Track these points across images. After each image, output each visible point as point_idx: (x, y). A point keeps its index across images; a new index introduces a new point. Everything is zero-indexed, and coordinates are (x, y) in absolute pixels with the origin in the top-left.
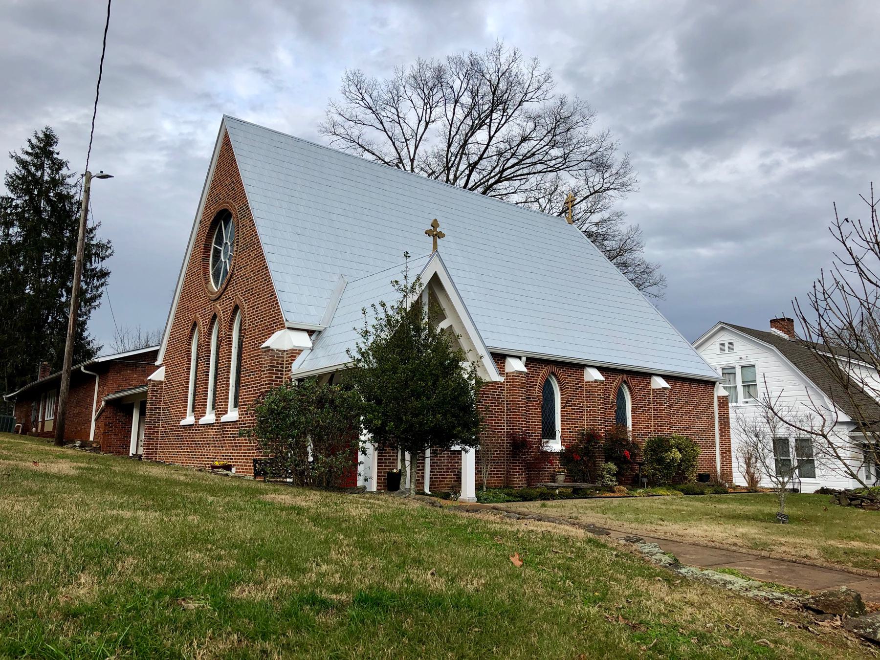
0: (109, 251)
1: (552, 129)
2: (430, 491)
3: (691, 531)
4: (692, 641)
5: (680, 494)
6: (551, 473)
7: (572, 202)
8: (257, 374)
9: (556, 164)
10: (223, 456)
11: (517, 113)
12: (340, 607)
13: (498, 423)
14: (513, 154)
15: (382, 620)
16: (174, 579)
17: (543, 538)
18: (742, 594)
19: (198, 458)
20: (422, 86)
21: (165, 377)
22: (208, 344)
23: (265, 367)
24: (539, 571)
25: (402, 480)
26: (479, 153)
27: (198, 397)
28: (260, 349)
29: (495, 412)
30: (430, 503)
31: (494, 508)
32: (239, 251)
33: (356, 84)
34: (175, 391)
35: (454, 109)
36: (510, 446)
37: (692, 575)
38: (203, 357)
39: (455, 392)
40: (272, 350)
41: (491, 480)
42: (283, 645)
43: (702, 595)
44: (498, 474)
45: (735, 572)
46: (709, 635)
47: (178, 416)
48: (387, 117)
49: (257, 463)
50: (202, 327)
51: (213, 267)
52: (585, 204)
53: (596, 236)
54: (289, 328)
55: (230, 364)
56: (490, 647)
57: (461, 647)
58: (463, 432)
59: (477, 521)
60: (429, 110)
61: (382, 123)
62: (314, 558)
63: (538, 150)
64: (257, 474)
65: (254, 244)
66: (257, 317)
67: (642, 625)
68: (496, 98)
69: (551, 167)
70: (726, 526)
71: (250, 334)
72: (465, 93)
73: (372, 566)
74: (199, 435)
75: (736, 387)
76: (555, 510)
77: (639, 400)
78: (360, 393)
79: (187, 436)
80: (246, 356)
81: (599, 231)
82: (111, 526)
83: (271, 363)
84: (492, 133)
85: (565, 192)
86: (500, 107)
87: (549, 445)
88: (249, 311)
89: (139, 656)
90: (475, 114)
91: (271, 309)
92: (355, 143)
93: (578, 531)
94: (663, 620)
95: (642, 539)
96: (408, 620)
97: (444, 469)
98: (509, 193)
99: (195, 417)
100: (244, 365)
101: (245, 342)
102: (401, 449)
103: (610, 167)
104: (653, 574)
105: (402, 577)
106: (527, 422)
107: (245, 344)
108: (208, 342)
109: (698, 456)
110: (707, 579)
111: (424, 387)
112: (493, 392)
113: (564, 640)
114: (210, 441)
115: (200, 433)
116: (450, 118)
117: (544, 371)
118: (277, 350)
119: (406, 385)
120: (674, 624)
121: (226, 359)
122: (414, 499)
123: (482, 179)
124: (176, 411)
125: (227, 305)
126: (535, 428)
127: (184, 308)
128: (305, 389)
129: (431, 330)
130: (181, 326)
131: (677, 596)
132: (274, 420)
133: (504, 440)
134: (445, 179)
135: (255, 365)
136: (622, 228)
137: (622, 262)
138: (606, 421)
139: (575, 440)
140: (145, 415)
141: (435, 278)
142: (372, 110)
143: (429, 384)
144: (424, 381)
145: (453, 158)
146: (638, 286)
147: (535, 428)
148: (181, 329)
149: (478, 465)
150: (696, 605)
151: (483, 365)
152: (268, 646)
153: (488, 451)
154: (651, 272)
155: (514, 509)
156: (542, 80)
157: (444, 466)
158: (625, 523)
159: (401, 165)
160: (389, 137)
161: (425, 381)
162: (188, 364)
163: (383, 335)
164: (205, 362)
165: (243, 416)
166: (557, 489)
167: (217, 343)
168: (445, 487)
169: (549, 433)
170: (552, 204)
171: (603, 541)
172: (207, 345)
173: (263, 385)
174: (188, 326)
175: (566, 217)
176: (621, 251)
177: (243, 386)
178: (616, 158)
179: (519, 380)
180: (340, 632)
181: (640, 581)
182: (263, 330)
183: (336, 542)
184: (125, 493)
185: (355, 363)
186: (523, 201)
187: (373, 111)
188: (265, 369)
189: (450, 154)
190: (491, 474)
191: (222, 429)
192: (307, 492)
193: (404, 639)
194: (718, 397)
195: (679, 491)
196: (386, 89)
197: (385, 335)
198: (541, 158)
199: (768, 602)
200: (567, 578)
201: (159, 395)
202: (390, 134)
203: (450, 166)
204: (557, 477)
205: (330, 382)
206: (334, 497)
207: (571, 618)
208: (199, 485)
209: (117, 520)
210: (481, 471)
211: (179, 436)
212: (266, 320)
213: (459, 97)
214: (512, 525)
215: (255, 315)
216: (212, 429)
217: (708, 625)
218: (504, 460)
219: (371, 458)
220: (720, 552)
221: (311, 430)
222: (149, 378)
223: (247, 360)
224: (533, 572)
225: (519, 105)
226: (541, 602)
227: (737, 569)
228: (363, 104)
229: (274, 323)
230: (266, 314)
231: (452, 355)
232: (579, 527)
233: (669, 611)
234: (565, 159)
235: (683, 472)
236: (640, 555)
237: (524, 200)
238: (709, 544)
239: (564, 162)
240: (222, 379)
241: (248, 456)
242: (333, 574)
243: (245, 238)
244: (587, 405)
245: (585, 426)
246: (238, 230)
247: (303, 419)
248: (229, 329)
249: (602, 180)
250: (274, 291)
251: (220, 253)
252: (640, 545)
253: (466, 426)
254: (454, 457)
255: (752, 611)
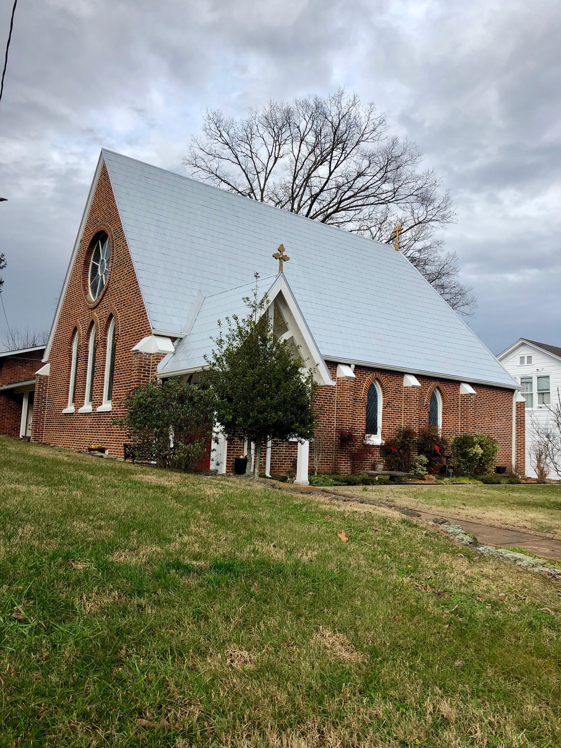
0: (3, 263)
1: (384, 166)
2: (270, 475)
3: (488, 515)
4: (487, 607)
5: (480, 483)
6: (372, 463)
7: (399, 231)
8: (127, 373)
9: (386, 198)
10: (98, 440)
11: (354, 151)
12: (200, 571)
13: (329, 420)
14: (350, 188)
15: (234, 583)
16: (65, 544)
17: (365, 518)
18: (529, 569)
19: (77, 441)
20: (272, 125)
21: (50, 372)
22: (87, 346)
23: (134, 367)
24: (362, 545)
25: (248, 466)
26: (320, 186)
27: (78, 390)
28: (130, 352)
29: (327, 410)
30: (271, 485)
31: (324, 491)
32: (113, 267)
33: (216, 122)
34: (59, 385)
35: (300, 147)
36: (338, 439)
37: (488, 553)
38: (82, 357)
39: (294, 394)
40: (141, 353)
41: (322, 467)
42: (155, 601)
43: (496, 569)
44: (327, 462)
45: (524, 550)
46: (500, 602)
47: (61, 405)
48: (242, 152)
49: (127, 447)
50: (81, 331)
51: (91, 281)
52: (410, 233)
53: (419, 261)
54: (155, 335)
55: (105, 363)
56: (322, 608)
57: (298, 607)
58: (300, 427)
59: (312, 501)
60: (278, 147)
61: (237, 157)
62: (177, 530)
63: (372, 184)
64: (126, 456)
65: (127, 262)
66: (128, 324)
67: (446, 593)
68: (336, 138)
69: (382, 200)
70: (518, 511)
71: (122, 339)
72: (310, 133)
73: (225, 538)
74: (78, 422)
75: (532, 394)
76: (374, 493)
77: (449, 403)
78: (215, 392)
79: (68, 422)
80: (119, 357)
81: (421, 257)
82: (11, 498)
83: (140, 364)
84: (332, 169)
85: (393, 222)
86: (340, 146)
87: (371, 439)
88: (122, 319)
89: (41, 606)
90: (318, 151)
91: (140, 318)
92: (213, 175)
93: (394, 513)
94: (463, 590)
95: (448, 521)
96: (255, 583)
97: (282, 456)
98: (345, 222)
99: (75, 407)
100: (116, 365)
101: (118, 345)
102: (248, 440)
103: (433, 201)
104: (456, 551)
105: (249, 548)
106: (353, 419)
107: (118, 347)
108: (86, 344)
109: (496, 452)
110: (501, 556)
111: (269, 388)
112: (325, 393)
113: (381, 604)
114: (87, 427)
115: (79, 420)
116: (296, 155)
117: (369, 377)
118: (145, 353)
119: (254, 387)
120: (473, 593)
121: (101, 359)
122: (258, 481)
123: (322, 209)
124: (59, 401)
125: (103, 313)
126: (360, 424)
127: (66, 315)
128: (169, 387)
129: (275, 340)
130: (64, 330)
131: (476, 570)
132: (142, 412)
133: (333, 434)
134: (290, 208)
135: (126, 365)
136: (442, 254)
137: (440, 284)
138: (420, 420)
139: (394, 436)
140: (33, 404)
141: (280, 295)
142: (229, 146)
143: (273, 386)
144: (268, 383)
145: (298, 190)
146: (453, 306)
147: (360, 424)
148: (63, 332)
149: (311, 454)
150: (491, 577)
151: (319, 371)
152: (143, 601)
153: (319, 443)
154: (464, 294)
155: (340, 492)
156: (377, 123)
157: (282, 454)
158: (433, 507)
159: (252, 195)
160: (243, 169)
161: (270, 384)
162: (70, 362)
163: (235, 344)
164: (84, 361)
165: (115, 408)
166: (377, 476)
167: (94, 345)
168: (283, 472)
169: (372, 429)
170: (382, 232)
171: (415, 522)
172: (86, 347)
173: (132, 382)
174: (70, 330)
175: (394, 244)
176: (440, 275)
177: (116, 382)
178: (439, 193)
179: (348, 385)
180: (201, 592)
181: (445, 557)
182: (133, 336)
183: (194, 517)
184: (20, 469)
185: (211, 366)
186: (356, 229)
187: (230, 147)
188: (135, 369)
189: (295, 186)
190: (322, 462)
191: (97, 417)
192: (169, 473)
193: (252, 599)
194: (516, 402)
195: (479, 480)
196: (241, 127)
197: (237, 343)
198: (373, 192)
199: (551, 577)
200: (385, 552)
201: (44, 388)
202: (244, 167)
203: (294, 196)
204: (377, 466)
205: (189, 381)
206: (191, 478)
207: (388, 586)
208: (81, 465)
209: (15, 493)
210: (313, 460)
211: (61, 422)
212: (136, 327)
213: (304, 136)
214: (339, 506)
215: (126, 322)
216: (89, 417)
217: (500, 595)
218: (332, 450)
219: (222, 446)
220: (511, 533)
221: (173, 422)
222: (36, 373)
223: (120, 361)
224: (357, 546)
225: (357, 144)
226: (363, 572)
227: (528, 548)
228: (221, 140)
229: (142, 330)
230: (136, 322)
231: (292, 363)
232: (395, 509)
233: (469, 582)
234: (395, 193)
235: (483, 464)
236: (445, 534)
237: (358, 228)
238: (503, 526)
239: (393, 196)
240: (98, 376)
241: (119, 441)
242: (193, 544)
243: (119, 256)
244: (404, 406)
245: (403, 424)
246: (113, 249)
247: (166, 412)
248: (105, 334)
249: (425, 212)
250: (143, 303)
251: (98, 268)
252: (446, 526)
253: (303, 423)
254: (291, 447)
255: (537, 585)
